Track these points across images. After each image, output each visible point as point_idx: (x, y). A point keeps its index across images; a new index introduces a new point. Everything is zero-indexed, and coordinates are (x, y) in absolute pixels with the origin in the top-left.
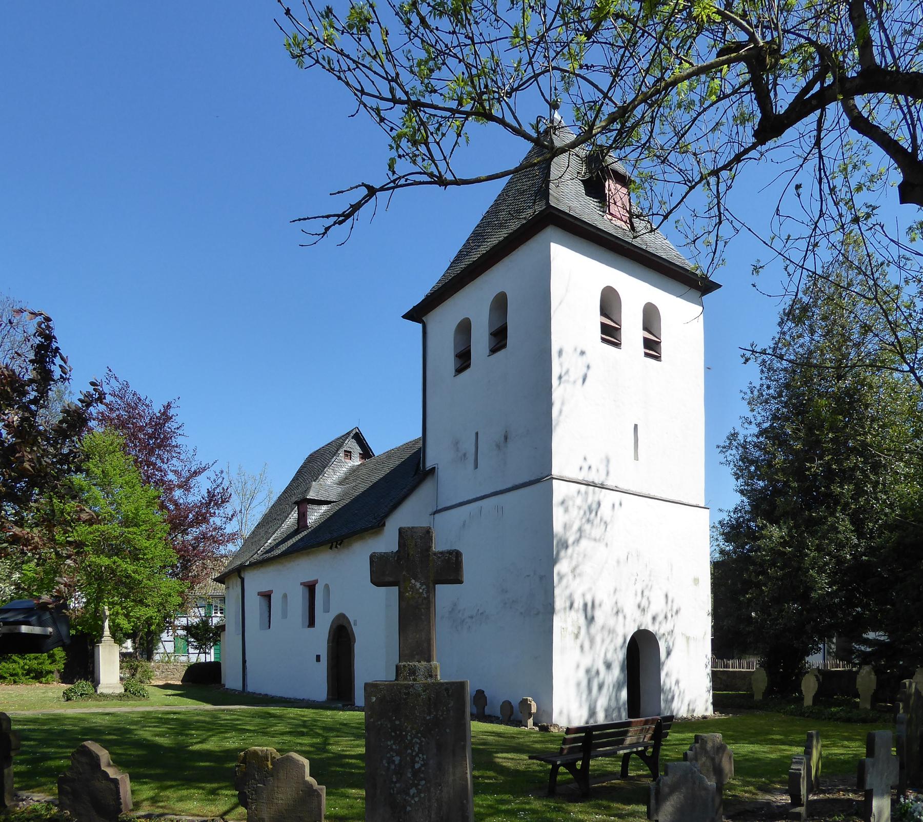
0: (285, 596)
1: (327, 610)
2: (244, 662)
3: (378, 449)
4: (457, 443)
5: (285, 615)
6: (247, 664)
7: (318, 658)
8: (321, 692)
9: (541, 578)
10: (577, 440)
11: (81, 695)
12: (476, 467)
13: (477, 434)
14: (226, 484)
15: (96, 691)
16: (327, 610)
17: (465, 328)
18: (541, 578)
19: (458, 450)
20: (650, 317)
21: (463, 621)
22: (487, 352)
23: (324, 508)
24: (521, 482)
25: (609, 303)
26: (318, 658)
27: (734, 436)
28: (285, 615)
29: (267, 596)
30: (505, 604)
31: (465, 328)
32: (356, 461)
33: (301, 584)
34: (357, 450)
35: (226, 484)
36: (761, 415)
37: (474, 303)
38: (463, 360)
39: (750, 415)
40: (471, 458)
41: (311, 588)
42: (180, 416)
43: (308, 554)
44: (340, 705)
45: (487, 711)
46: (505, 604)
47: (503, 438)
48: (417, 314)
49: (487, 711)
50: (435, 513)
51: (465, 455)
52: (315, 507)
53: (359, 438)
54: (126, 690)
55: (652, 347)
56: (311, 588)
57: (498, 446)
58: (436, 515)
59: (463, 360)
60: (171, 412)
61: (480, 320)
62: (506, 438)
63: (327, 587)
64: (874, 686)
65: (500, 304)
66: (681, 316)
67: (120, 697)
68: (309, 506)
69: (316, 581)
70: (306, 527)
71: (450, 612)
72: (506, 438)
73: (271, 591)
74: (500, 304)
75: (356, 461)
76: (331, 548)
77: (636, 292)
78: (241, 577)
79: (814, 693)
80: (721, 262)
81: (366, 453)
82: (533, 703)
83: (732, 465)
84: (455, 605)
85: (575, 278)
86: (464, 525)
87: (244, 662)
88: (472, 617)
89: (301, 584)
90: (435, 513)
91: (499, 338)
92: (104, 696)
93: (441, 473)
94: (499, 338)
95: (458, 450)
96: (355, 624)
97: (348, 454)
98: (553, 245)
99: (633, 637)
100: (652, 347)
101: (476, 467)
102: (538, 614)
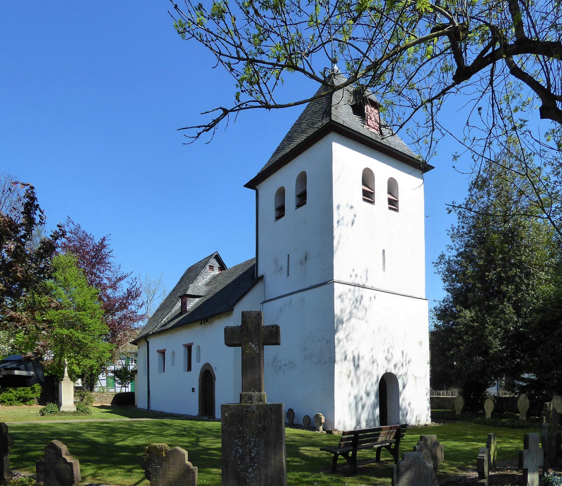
1: (198, 361)
2: (149, 392)
3: (229, 265)
4: (277, 261)
5: (173, 364)
6: (151, 393)
7: (193, 390)
8: (195, 410)
9: (327, 341)
11: (51, 412)
12: (288, 275)
14: (138, 286)
15: (59, 410)
16: (198, 361)
17: (281, 193)
18: (327, 341)
19: (277, 265)
20: (392, 186)
22: (295, 207)
23: (197, 300)
25: (367, 178)
26: (193, 390)
28: (173, 364)
31: (281, 193)
33: (183, 345)
34: (217, 265)
35: (138, 286)
37: (286, 178)
38: (280, 211)
39: (452, 244)
41: (189, 348)
42: (111, 245)
43: (187, 327)
44: (206, 418)
45: (295, 422)
46: (306, 357)
47: (304, 258)
48: (252, 184)
51: (281, 268)
52: (192, 299)
54: (77, 409)
55: (393, 204)
56: (189, 348)
57: (301, 263)
59: (280, 211)
60: (106, 243)
61: (289, 186)
62: (306, 258)
63: (198, 347)
64: (528, 406)
65: (302, 178)
66: (410, 185)
67: (74, 413)
68: (188, 299)
69: (192, 344)
70: (186, 311)
72: (306, 258)
74: (302, 178)
75: (216, 272)
77: (384, 171)
78: (147, 341)
79: (491, 411)
80: (434, 153)
81: (222, 267)
82: (323, 417)
85: (347, 162)
86: (281, 310)
87: (149, 392)
88: (285, 365)
91: (302, 198)
92: (65, 413)
93: (268, 279)
94: (302, 198)
95: (277, 265)
96: (216, 369)
97: (211, 267)
98: (333, 143)
100: (393, 204)
101: (288, 275)
102: (325, 363)
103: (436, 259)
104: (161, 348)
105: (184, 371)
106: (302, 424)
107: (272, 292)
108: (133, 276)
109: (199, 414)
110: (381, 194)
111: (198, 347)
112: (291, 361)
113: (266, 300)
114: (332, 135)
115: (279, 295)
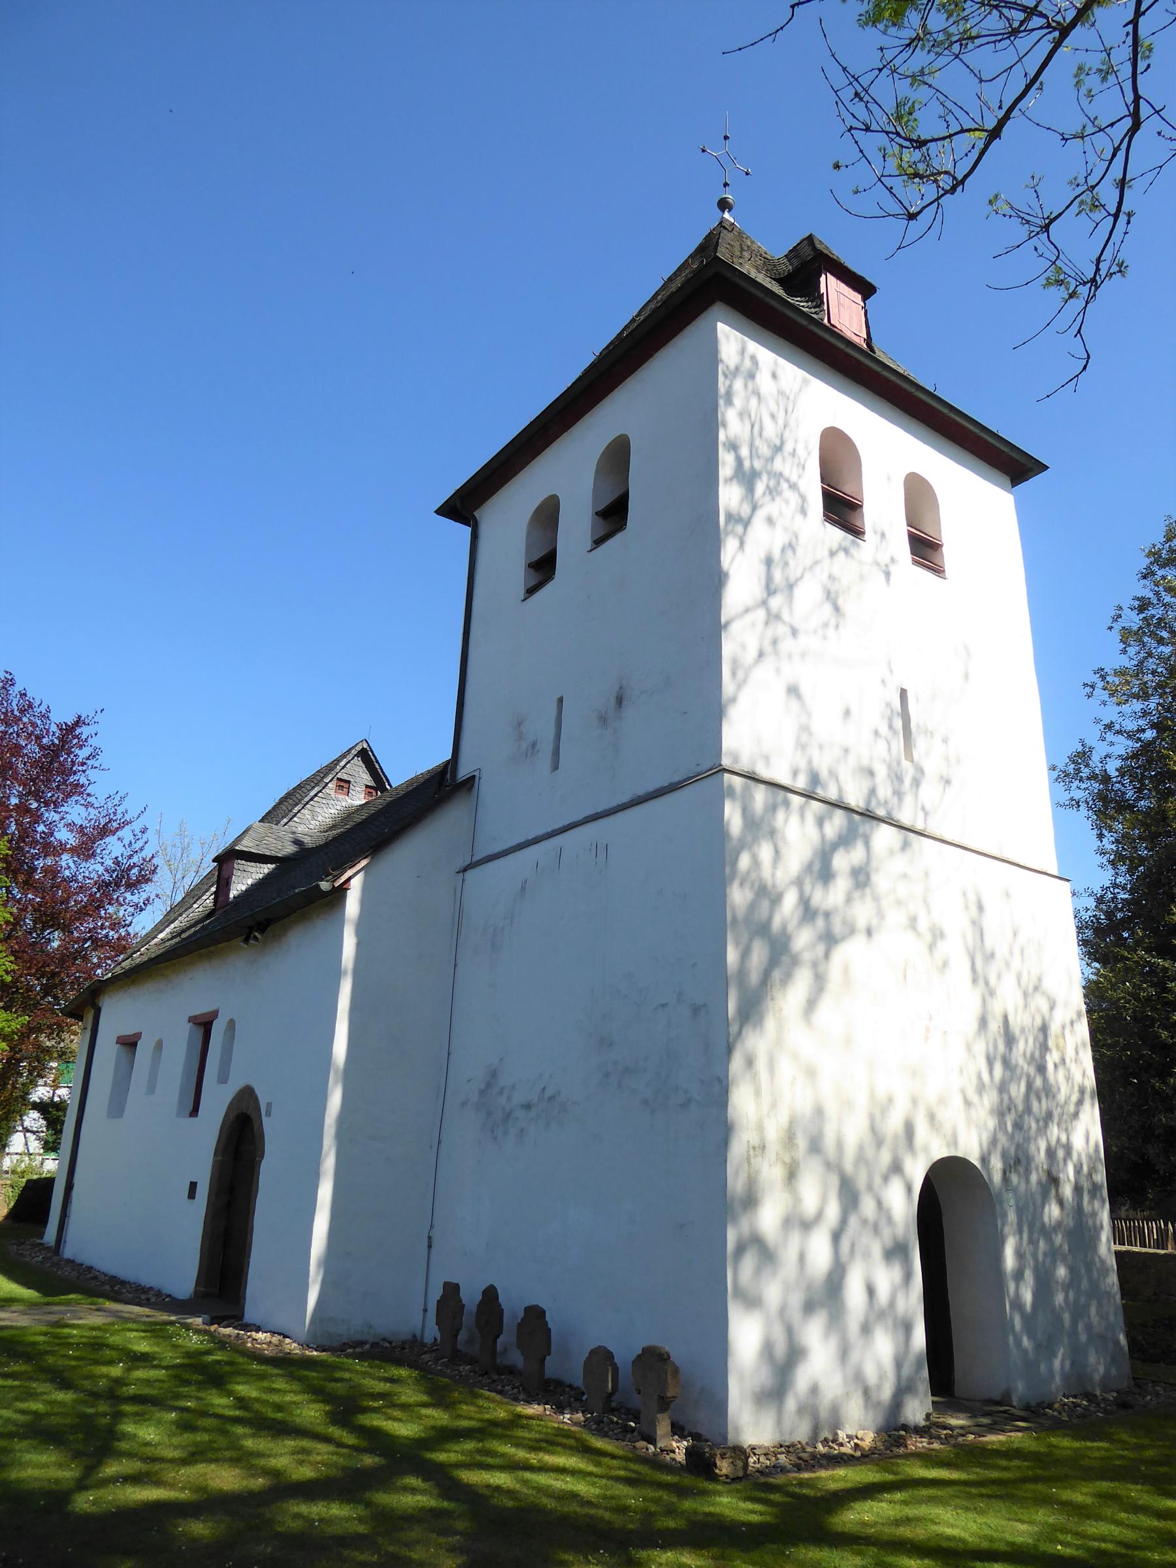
0: (159, 1045)
1: (223, 1079)
4: (520, 724)
5: (151, 1089)
6: (75, 1193)
9: (696, 1010)
10: (782, 705)
12: (555, 766)
13: (561, 700)
16: (223, 1079)
17: (548, 515)
18: (696, 1010)
19: (520, 737)
20: (918, 495)
21: (508, 1115)
22: (589, 544)
24: (651, 788)
25: (837, 453)
27: (1082, 756)
28: (151, 1089)
29: (130, 1043)
30: (607, 1075)
31: (548, 515)
32: (358, 798)
33: (191, 1019)
36: (1129, 715)
37: (568, 472)
38: (543, 567)
40: (546, 748)
41: (204, 1025)
42: (102, 737)
43: (210, 956)
45: (552, 1368)
46: (607, 1075)
47: (613, 702)
48: (463, 506)
49: (552, 1368)
50: (465, 870)
51: (534, 745)
53: (366, 757)
55: (925, 549)
56: (204, 1025)
57: (603, 720)
58: (470, 874)
59: (543, 567)
60: (84, 731)
61: (576, 484)
62: (620, 700)
63: (231, 1024)
65: (618, 456)
66: (974, 504)
69: (214, 1014)
71: (482, 1092)
72: (620, 700)
73: (138, 1036)
74: (618, 456)
76: (246, 941)
77: (890, 452)
80: (1115, 269)
81: (379, 780)
83: (1083, 806)
84: (494, 1074)
85: (771, 400)
86: (523, 889)
88: (528, 1107)
89: (191, 1019)
90: (465, 870)
91: (613, 515)
93: (487, 789)
94: (613, 515)
95: (520, 737)
96: (268, 1114)
97: (344, 785)
99: (927, 1179)
100: (925, 549)
101: (555, 766)
102: (685, 1105)
103: (1062, 762)
104: (129, 1031)
105: (178, 1115)
106: (579, 1382)
107: (497, 830)
108: (137, 826)
109: (196, 1292)
110: (882, 507)
111: (231, 1024)
112: (547, 1094)
113: (476, 859)
114: (718, 309)
115: (522, 840)
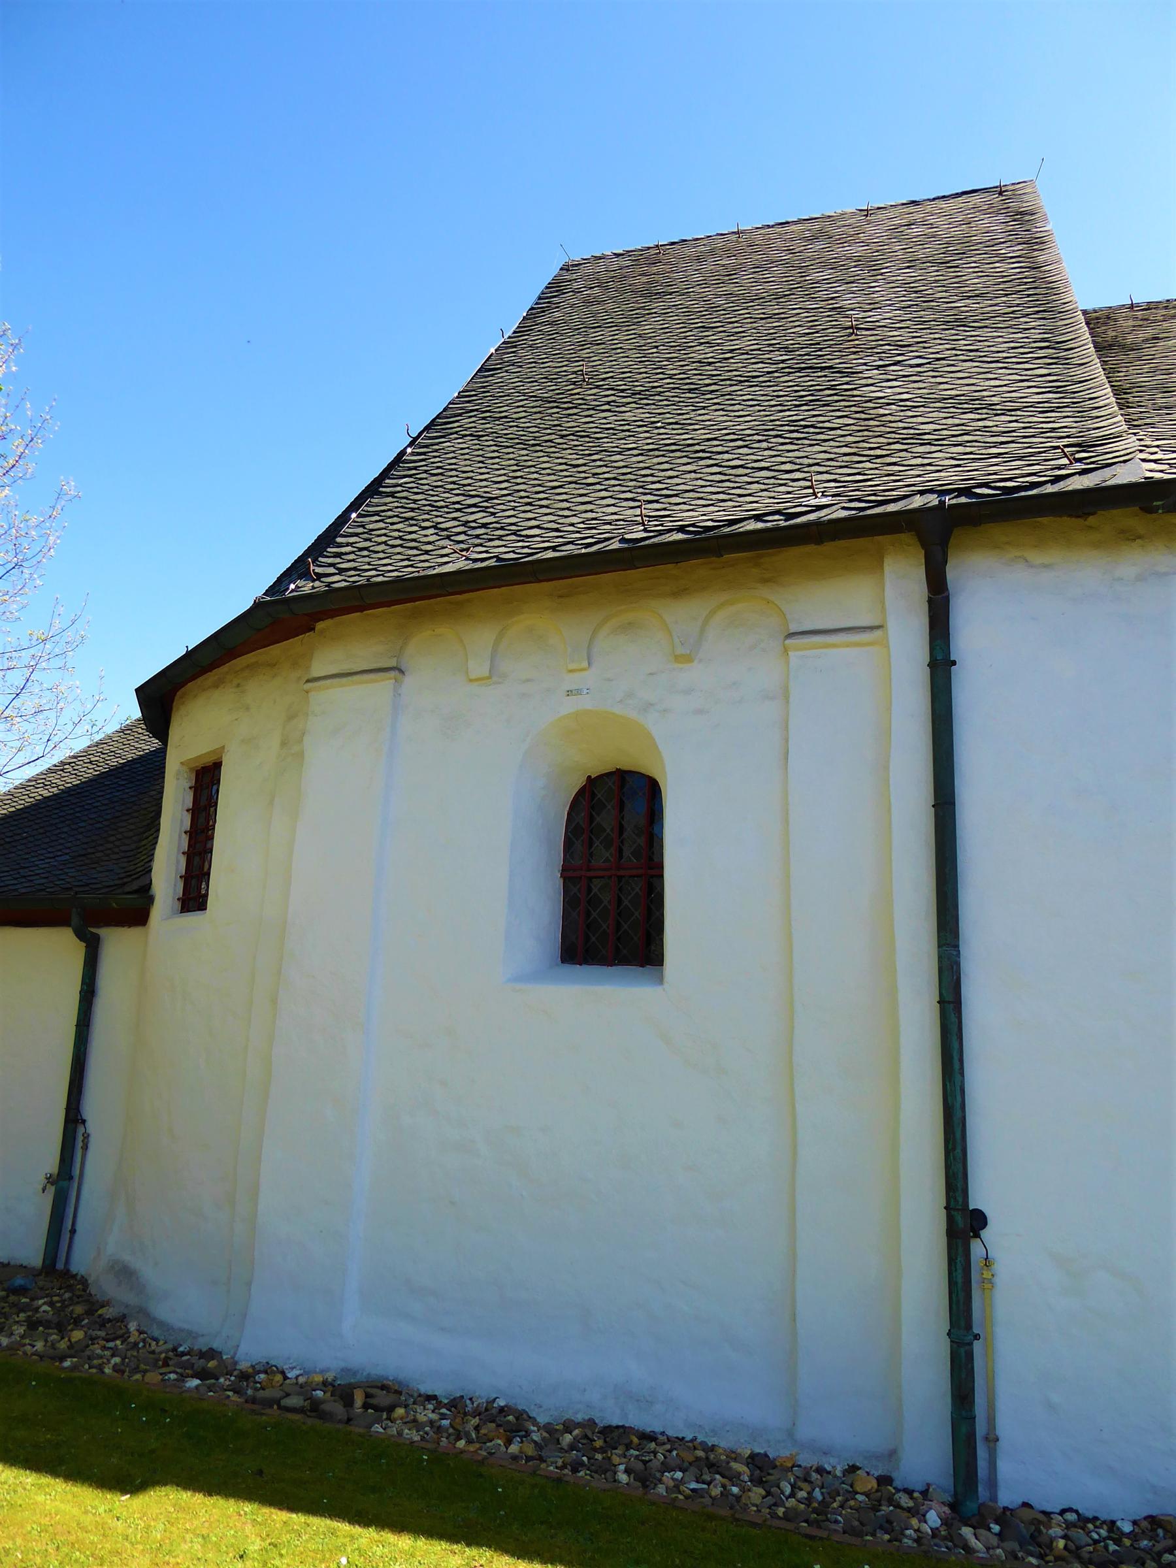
87: (74, 1118)
